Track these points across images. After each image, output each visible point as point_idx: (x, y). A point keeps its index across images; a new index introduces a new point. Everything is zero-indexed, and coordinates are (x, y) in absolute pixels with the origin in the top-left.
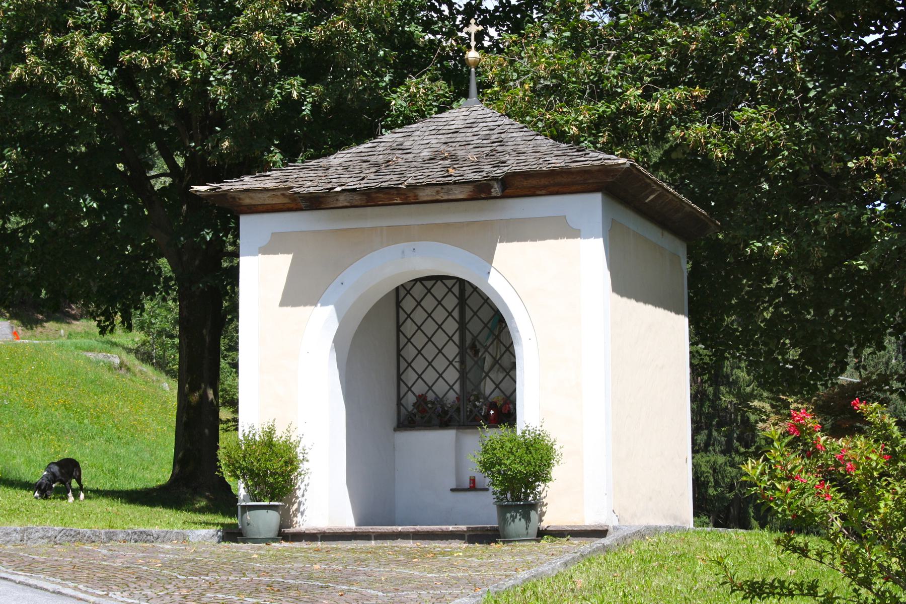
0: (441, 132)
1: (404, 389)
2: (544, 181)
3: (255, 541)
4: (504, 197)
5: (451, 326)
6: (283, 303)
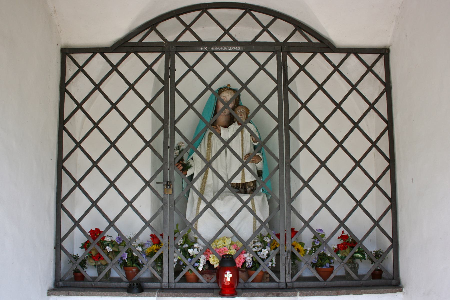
1: (66, 224)
5: (147, 125)
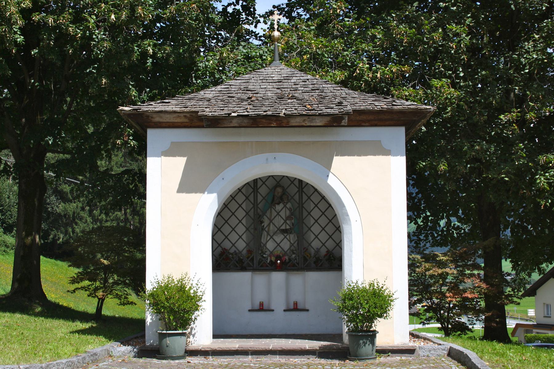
0: (268, 81)
2: (371, 117)
3: (173, 358)
4: (348, 126)
6: (180, 191)
